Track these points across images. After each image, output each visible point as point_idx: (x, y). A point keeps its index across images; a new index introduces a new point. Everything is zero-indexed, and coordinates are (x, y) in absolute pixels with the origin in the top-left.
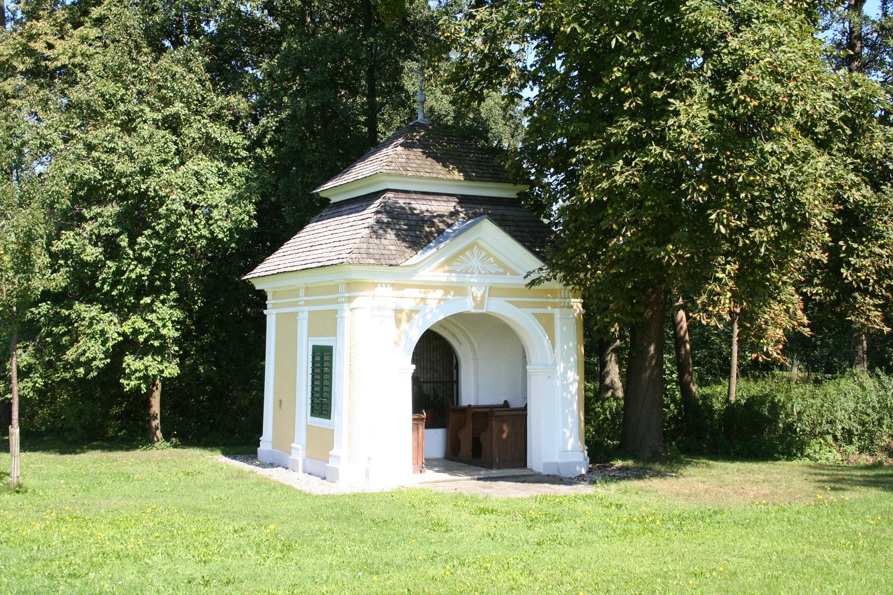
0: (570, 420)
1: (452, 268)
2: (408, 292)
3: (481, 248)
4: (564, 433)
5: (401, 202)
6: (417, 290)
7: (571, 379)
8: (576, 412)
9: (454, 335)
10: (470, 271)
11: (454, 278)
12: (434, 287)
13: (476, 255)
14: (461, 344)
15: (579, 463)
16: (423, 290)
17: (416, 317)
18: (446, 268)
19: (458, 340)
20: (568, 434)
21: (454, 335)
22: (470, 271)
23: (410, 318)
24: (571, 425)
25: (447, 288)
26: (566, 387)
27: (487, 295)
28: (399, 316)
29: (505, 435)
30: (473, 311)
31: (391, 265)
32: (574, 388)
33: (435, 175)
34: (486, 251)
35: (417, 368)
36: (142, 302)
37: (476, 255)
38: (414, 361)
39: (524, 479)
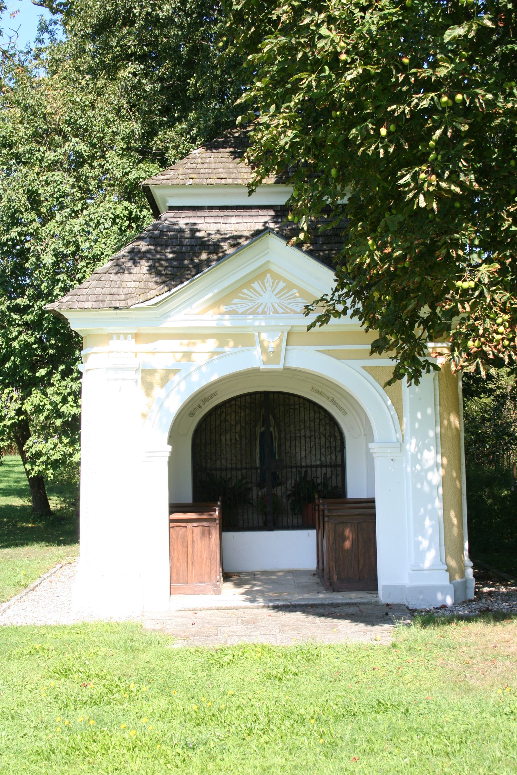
0: (427, 522)
1: (231, 308)
2: (161, 345)
3: (277, 277)
4: (419, 543)
5: (182, 223)
6: (178, 342)
7: (431, 463)
8: (441, 513)
9: (334, 402)
10: (260, 310)
11: (227, 322)
12: (203, 336)
13: (269, 288)
14: (345, 413)
15: (442, 589)
16: (185, 341)
17: (176, 378)
18: (223, 308)
19: (341, 409)
20: (425, 543)
21: (334, 402)
22: (260, 310)
23: (165, 381)
24: (430, 531)
25: (222, 337)
26: (420, 477)
27: (284, 343)
28: (149, 379)
29: (347, 544)
30: (263, 367)
31: (117, 308)
32: (436, 477)
33: (230, 181)
34: (285, 280)
35: (173, 449)
36: (37, 375)
37: (269, 288)
38: (169, 443)
39: (322, 611)
